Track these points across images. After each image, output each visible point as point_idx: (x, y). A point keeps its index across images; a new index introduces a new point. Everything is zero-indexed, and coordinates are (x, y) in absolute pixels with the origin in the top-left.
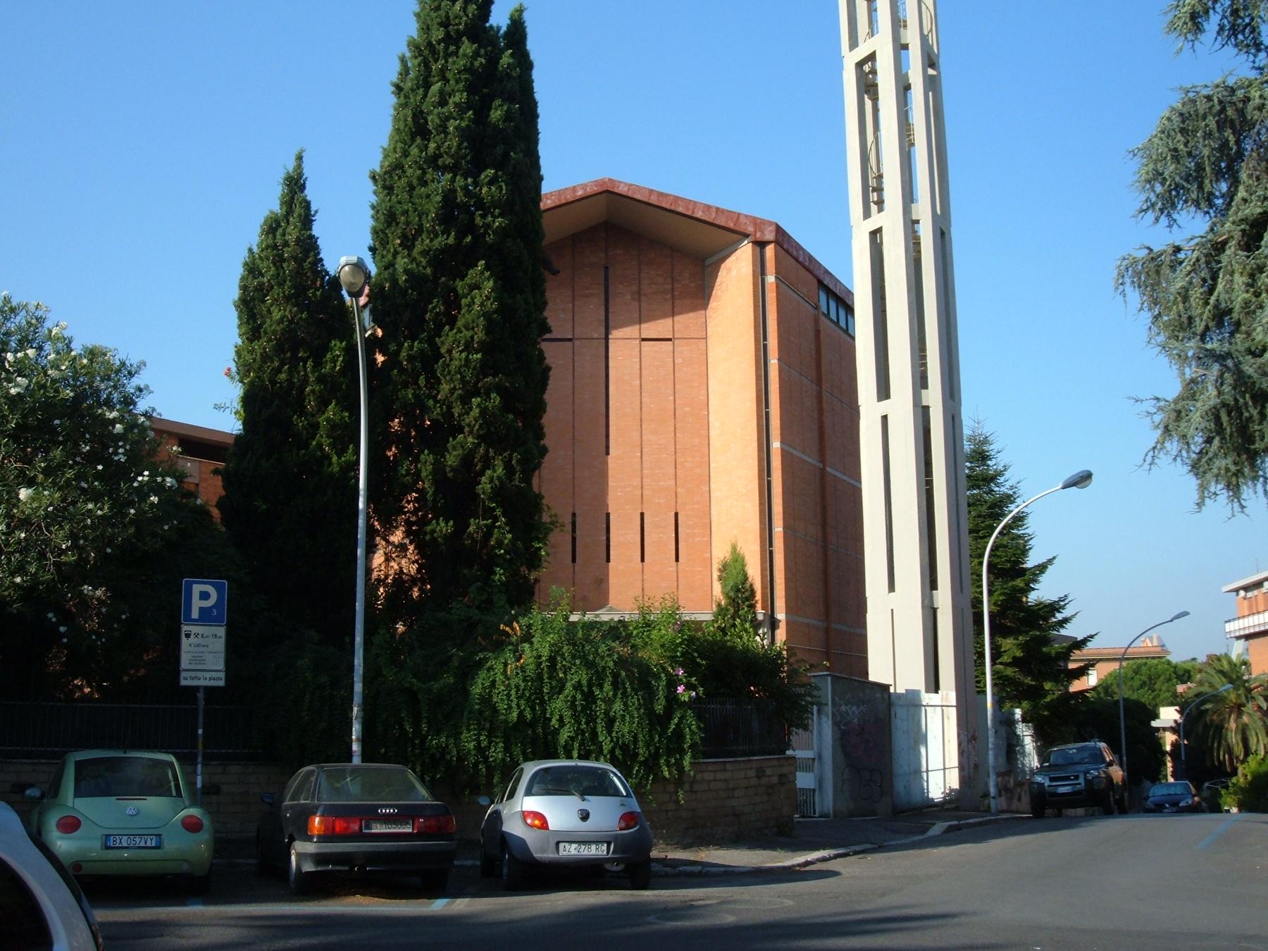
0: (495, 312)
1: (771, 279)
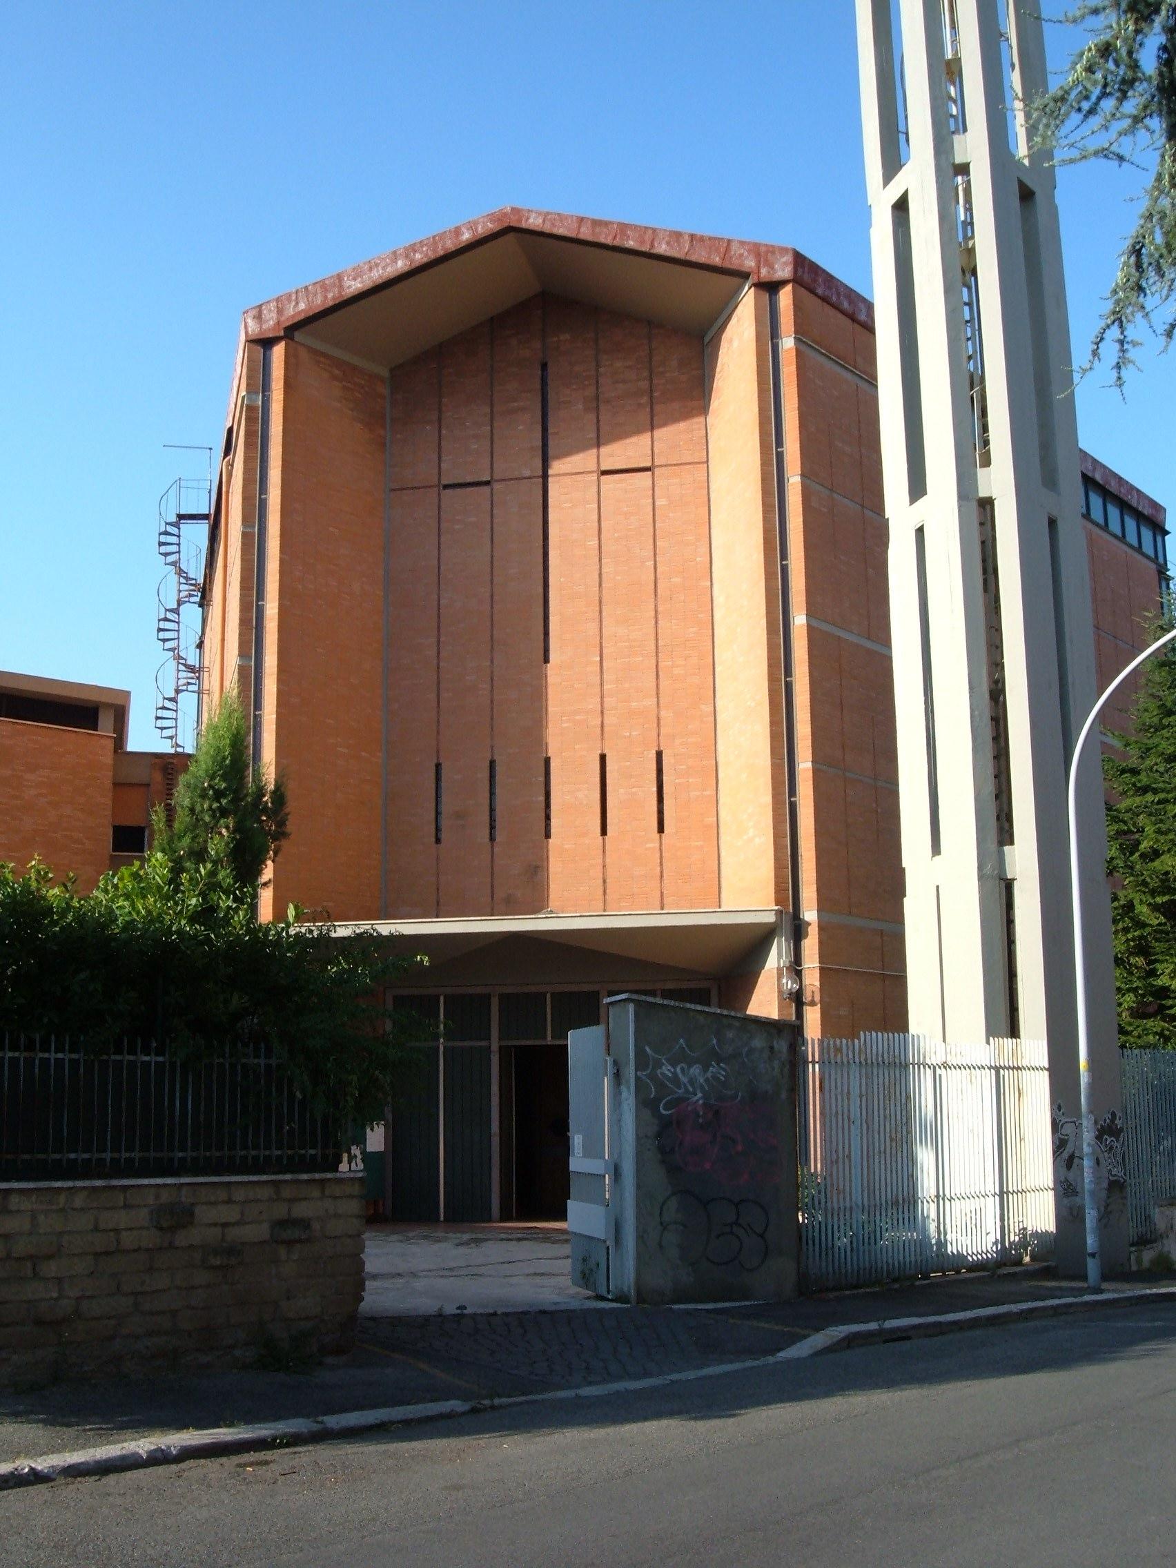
1: (788, 343)
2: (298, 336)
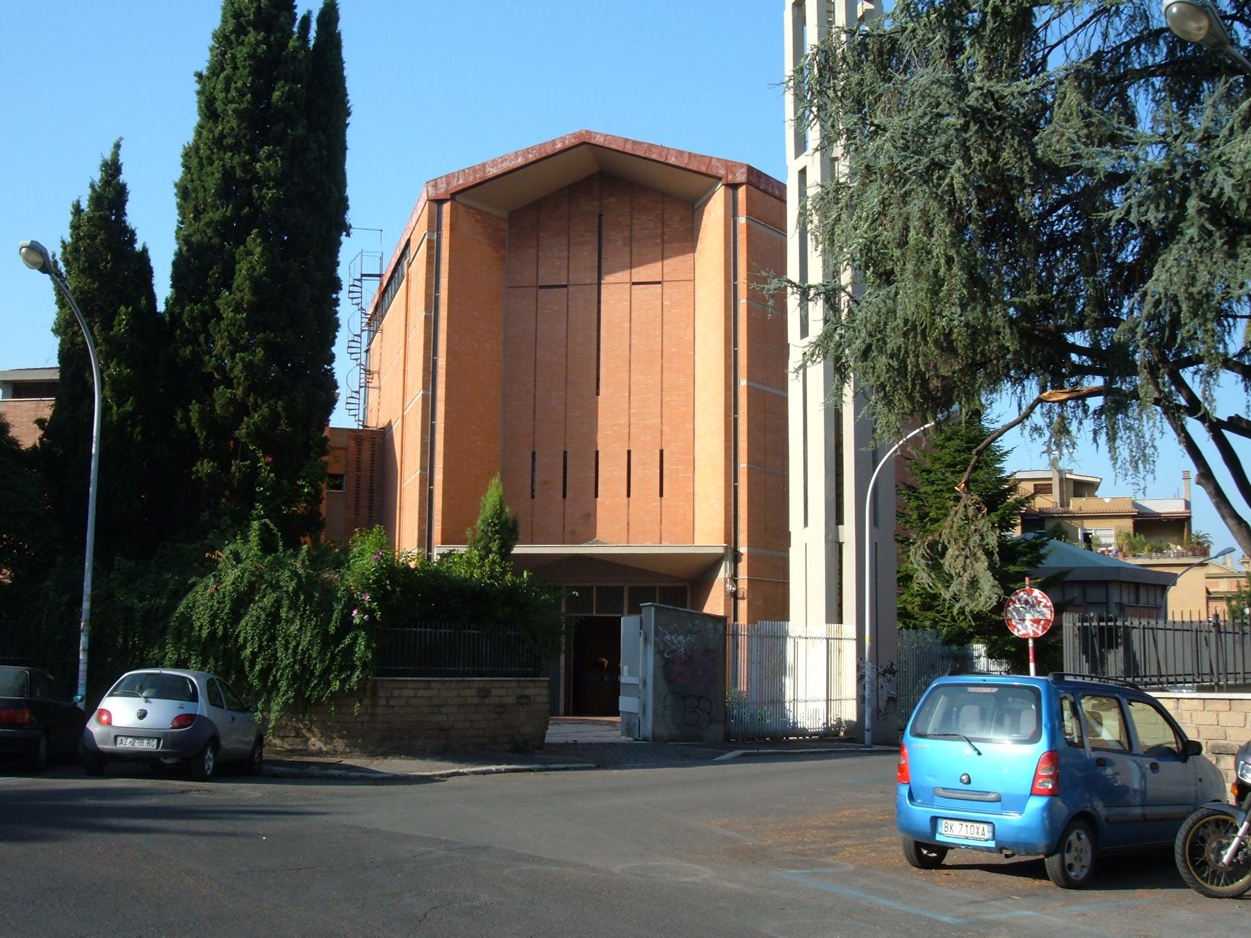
0: (265, 274)
1: (742, 220)
2: (458, 198)
